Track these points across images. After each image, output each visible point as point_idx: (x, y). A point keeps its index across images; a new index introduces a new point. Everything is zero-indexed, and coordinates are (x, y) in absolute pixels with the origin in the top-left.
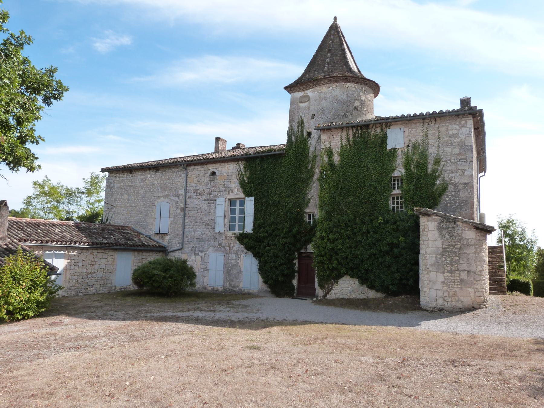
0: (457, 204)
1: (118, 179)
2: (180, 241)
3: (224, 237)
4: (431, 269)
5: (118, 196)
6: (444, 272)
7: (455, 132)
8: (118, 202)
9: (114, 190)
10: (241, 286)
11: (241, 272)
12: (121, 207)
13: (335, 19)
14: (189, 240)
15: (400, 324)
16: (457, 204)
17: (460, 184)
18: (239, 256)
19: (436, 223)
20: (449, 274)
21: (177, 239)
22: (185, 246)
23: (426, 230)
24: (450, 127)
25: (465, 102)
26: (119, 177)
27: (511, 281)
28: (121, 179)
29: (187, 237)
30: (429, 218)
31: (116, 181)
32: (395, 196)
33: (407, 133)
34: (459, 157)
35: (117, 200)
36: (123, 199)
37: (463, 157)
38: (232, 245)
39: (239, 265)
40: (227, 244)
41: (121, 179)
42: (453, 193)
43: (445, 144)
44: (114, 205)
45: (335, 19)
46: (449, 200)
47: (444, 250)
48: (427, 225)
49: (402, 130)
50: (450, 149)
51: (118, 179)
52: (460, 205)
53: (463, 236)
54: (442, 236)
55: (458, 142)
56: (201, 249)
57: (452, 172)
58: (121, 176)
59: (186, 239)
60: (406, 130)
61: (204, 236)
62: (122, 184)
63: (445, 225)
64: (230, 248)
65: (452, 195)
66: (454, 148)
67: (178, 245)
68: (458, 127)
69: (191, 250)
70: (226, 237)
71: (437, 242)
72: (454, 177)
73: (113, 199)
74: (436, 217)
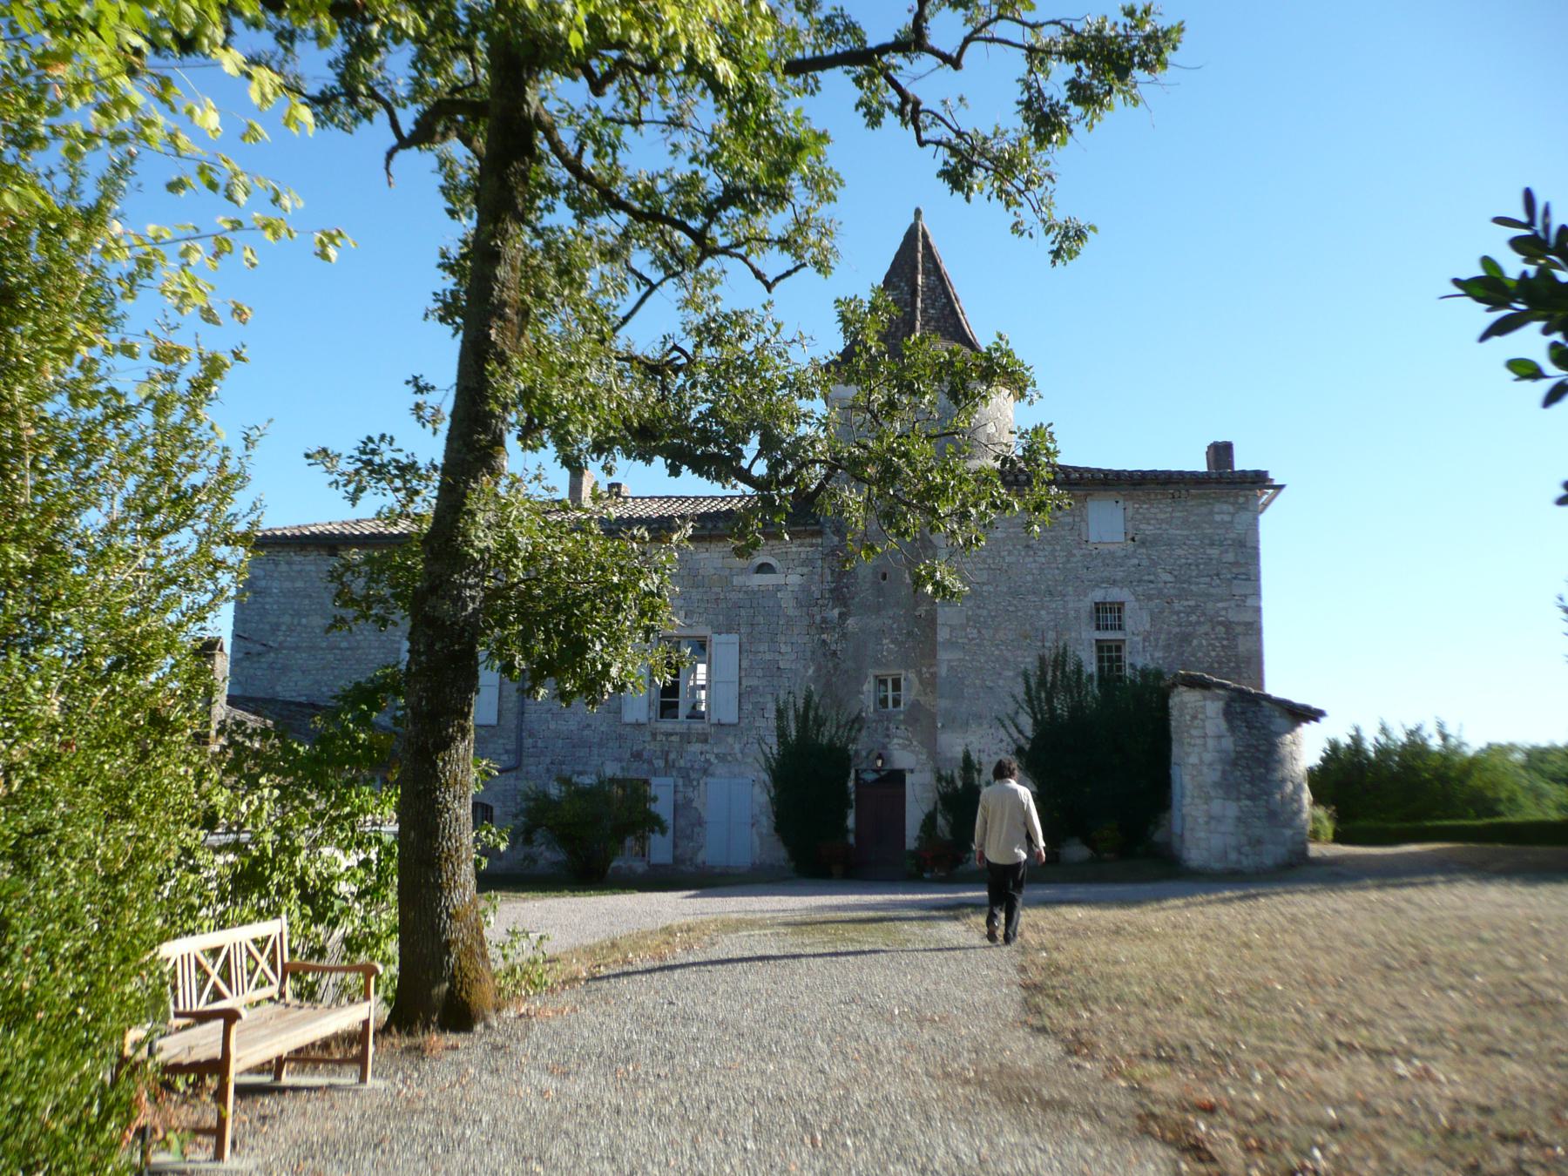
0: (1232, 664)
1: (283, 567)
2: (511, 746)
3: (648, 734)
4: (1213, 794)
5: (287, 619)
6: (1238, 799)
7: (1227, 518)
8: (285, 636)
9: (268, 600)
10: (701, 857)
11: (700, 822)
12: (297, 648)
13: (918, 213)
14: (540, 744)
15: (1124, 902)
16: (1232, 664)
17: (1238, 624)
18: (695, 783)
19: (1220, 704)
20: (1248, 802)
21: (500, 741)
22: (525, 761)
23: (1200, 716)
24: (1217, 507)
25: (1221, 452)
26: (289, 563)
27: (844, 750)
28: (296, 568)
29: (531, 735)
30: (1207, 693)
31: (276, 575)
32: (1113, 644)
33: (1130, 512)
34: (1235, 570)
35: (284, 628)
36: (305, 626)
37: (1243, 570)
38: (672, 756)
39: (694, 805)
40: (659, 753)
41: (296, 568)
42: (1225, 643)
43: (1207, 541)
44: (271, 643)
45: (918, 213)
46: (1217, 656)
47: (1239, 755)
48: (1204, 707)
49: (1121, 503)
50: (1217, 552)
51: (283, 567)
52: (1238, 667)
53: (1272, 728)
54: (1232, 729)
55: (1233, 540)
56: (579, 768)
57: (1222, 601)
58: (297, 559)
59: (528, 742)
60: (1129, 504)
61: (586, 732)
62: (299, 584)
63: (1237, 707)
64: (667, 761)
65: (1223, 646)
66: (1226, 552)
67: (505, 757)
68: (1231, 509)
69: (548, 770)
70: (654, 735)
71: (1223, 740)
72: (1226, 609)
73: (267, 627)
74: (1221, 692)
